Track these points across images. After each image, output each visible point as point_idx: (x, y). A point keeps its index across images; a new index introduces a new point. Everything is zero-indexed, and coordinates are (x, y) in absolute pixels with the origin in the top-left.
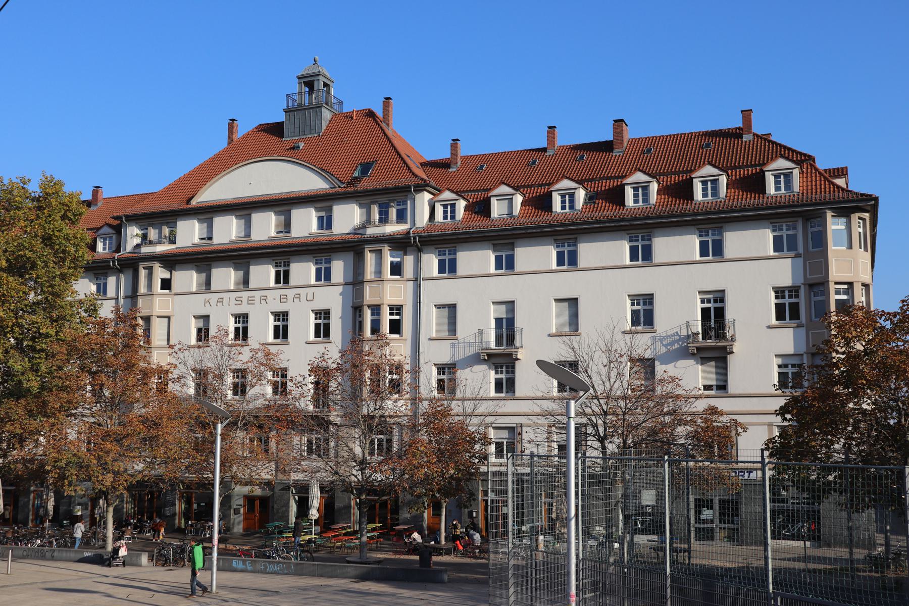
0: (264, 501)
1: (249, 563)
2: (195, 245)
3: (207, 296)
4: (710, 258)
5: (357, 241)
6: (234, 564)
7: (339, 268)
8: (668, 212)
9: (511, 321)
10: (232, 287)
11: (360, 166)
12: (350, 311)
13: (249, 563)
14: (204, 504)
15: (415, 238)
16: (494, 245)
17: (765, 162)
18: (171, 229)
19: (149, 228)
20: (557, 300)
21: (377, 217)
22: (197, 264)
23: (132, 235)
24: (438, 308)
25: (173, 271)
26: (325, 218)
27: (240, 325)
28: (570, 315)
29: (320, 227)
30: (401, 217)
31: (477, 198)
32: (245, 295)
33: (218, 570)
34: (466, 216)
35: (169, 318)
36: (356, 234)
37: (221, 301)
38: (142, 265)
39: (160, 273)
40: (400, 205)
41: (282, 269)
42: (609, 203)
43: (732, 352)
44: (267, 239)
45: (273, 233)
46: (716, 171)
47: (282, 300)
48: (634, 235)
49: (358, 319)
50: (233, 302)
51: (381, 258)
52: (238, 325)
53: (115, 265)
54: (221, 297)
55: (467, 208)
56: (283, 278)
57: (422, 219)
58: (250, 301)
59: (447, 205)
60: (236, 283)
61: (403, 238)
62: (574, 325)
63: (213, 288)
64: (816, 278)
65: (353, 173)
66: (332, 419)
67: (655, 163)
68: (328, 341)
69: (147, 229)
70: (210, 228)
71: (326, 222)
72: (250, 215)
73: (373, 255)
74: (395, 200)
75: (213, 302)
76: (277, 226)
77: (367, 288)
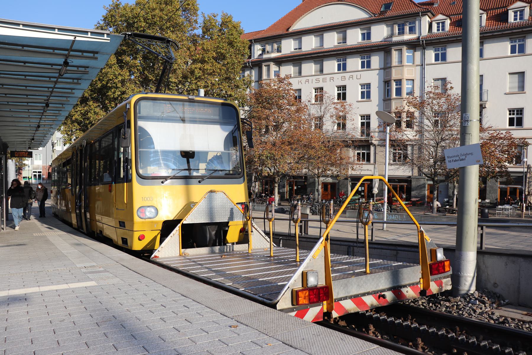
0: (333, 185)
1: (376, 215)
2: (292, 52)
3: (300, 79)
4: (440, 62)
5: (388, 45)
7: (376, 60)
8: (504, 28)
10: (313, 74)
11: (383, 5)
12: (382, 84)
13: (376, 215)
14: (300, 187)
15: (423, 41)
17: (507, 5)
20: (510, 74)
21: (397, 31)
23: (257, 49)
24: (435, 81)
26: (366, 34)
27: (341, 92)
29: (364, 39)
30: (412, 30)
31: (456, 19)
32: (321, 77)
34: (451, 29)
35: (413, 80)
36: (385, 41)
38: (264, 64)
39: (274, 68)
40: (411, 24)
41: (341, 63)
42: (498, 22)
44: (333, 47)
45: (336, 44)
46: (444, 17)
47: (342, 79)
49: (387, 88)
50: (314, 81)
51: (402, 54)
52: (339, 92)
53: (250, 65)
55: (451, 25)
56: (342, 68)
57: (425, 32)
58: (324, 80)
59: (439, 23)
60: (315, 72)
61: (415, 42)
62: (522, 87)
63: (303, 74)
64: (387, 78)
65: (380, 9)
66: (373, 142)
67: (484, 4)
68: (369, 100)
69: (265, 46)
70: (300, 43)
71: (367, 36)
72: (301, 38)
73: (397, 52)
74: (408, 21)
75: (303, 82)
76: (338, 40)
77: (394, 70)
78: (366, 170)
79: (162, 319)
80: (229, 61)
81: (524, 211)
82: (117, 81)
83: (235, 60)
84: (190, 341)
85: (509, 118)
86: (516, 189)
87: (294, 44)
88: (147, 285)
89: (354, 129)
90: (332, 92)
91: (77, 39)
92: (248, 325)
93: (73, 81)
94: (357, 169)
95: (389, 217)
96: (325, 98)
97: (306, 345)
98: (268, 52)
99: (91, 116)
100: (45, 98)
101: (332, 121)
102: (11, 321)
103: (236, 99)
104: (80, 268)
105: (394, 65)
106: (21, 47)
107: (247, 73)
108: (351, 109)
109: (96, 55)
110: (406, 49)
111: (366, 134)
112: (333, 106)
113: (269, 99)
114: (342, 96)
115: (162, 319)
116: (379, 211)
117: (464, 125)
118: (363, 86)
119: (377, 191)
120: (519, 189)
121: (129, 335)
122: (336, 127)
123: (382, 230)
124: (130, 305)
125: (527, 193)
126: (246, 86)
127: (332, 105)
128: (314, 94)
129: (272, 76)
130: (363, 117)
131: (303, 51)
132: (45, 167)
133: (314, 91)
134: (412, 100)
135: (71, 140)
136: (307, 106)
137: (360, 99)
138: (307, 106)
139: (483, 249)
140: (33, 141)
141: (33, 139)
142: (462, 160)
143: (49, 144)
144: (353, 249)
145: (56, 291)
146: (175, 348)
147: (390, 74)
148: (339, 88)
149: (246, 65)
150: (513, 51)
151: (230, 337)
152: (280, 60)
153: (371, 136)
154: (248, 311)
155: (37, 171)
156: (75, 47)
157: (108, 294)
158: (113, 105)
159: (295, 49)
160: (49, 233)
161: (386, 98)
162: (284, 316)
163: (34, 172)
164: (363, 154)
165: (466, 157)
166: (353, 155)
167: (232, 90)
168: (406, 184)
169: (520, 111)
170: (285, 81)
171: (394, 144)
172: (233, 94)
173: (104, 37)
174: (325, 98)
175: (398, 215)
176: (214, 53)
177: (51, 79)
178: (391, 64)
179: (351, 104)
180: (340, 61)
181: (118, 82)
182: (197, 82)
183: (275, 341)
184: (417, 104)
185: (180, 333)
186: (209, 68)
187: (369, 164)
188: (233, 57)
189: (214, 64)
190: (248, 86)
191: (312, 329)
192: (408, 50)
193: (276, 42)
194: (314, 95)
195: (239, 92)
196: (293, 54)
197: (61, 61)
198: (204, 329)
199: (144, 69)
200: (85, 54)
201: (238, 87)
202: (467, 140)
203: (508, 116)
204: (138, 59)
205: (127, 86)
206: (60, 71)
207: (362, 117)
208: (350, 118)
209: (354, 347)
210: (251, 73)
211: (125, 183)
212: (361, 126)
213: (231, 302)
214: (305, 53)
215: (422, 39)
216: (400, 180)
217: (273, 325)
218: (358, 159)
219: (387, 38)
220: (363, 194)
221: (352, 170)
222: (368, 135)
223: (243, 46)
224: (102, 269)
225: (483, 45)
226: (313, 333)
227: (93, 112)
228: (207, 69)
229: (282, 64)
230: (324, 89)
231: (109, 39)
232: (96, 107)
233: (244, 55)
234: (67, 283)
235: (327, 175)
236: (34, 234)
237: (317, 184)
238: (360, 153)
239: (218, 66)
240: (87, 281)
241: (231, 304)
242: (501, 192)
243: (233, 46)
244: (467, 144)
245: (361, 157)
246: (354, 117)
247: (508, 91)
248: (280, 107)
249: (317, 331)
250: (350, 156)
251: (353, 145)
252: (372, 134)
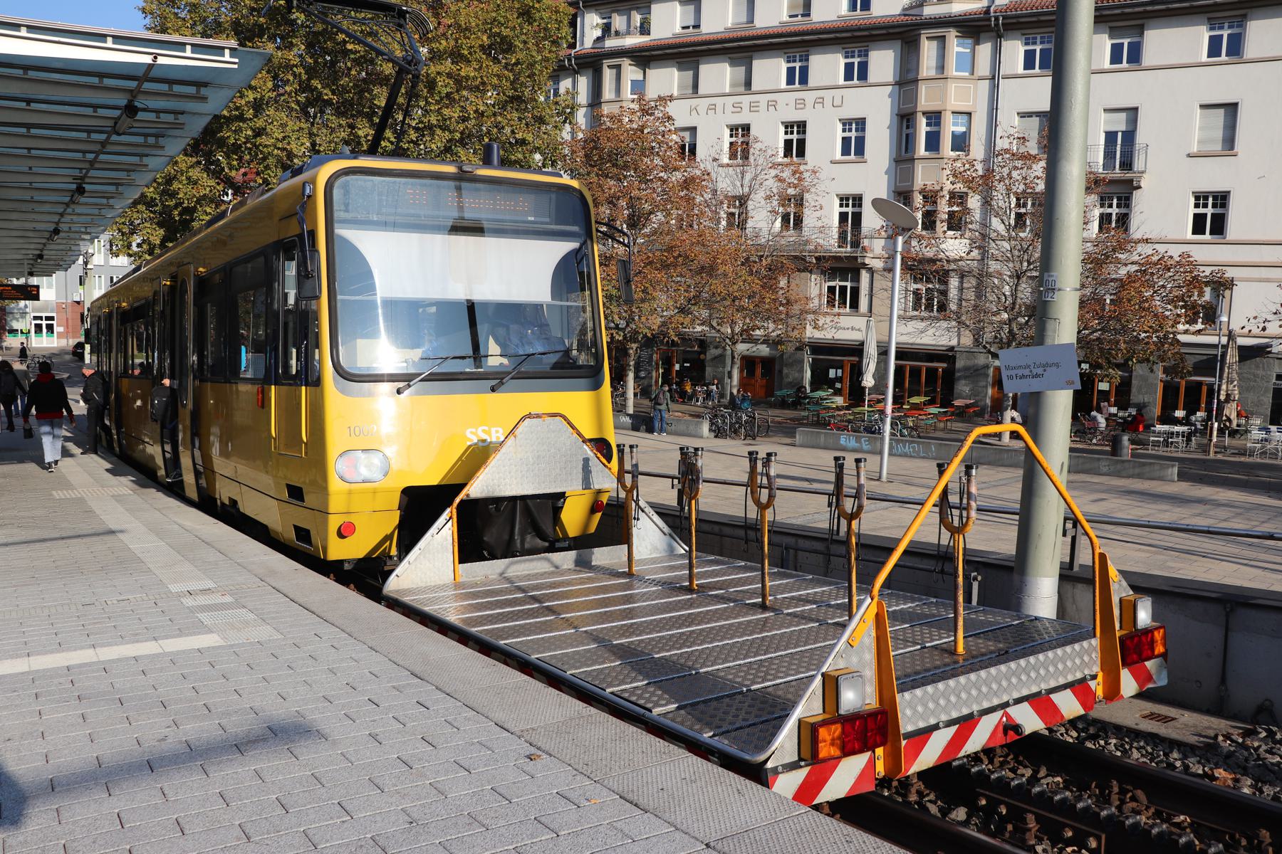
0: (768, 363)
1: (865, 441)
2: (676, 36)
5: (911, 25)
6: (843, 441)
7: (883, 62)
9: (1130, 136)
10: (727, 91)
13: (865, 441)
14: (688, 365)
15: (997, 19)
16: (1111, 28)
18: (645, 16)
19: (613, 15)
20: (1202, 106)
22: (678, 60)
24: (1021, 117)
25: (647, 70)
28: (1225, 127)
32: (746, 100)
33: (890, 454)
35: (969, 114)
37: (713, 107)
38: (606, 63)
39: (631, 73)
43: (1139, 187)
45: (785, 18)
48: (1031, 36)
49: (905, 131)
50: (729, 108)
52: (789, 137)
54: (822, 96)
58: (753, 107)
60: (732, 85)
63: (701, 91)
64: (907, 107)
66: (867, 261)
69: (610, 17)
73: (934, 43)
75: (702, 110)
77: (923, 89)
78: (848, 329)
79: (373, 736)
80: (521, 56)
81: (1215, 439)
82: (243, 102)
83: (534, 54)
84: (435, 792)
85: (1195, 214)
86: (1200, 384)
87: (683, 14)
88: (335, 644)
89: (822, 230)
90: (771, 138)
91: (161, 60)
92: (553, 754)
93: (146, 142)
94: (825, 326)
95: (898, 450)
96: (754, 154)
97: (667, 804)
98: (617, 33)
99: (179, 189)
100: (77, 173)
101: (770, 209)
102: (52, 738)
103: (537, 149)
104: (179, 595)
105: (925, 75)
106: (21, 72)
107: (565, 84)
108: (816, 180)
109: (204, 91)
110: (956, 37)
111: (852, 243)
112: (773, 172)
113: (617, 155)
114: (796, 148)
115: (373, 736)
116: (873, 433)
117: (1044, 299)
118: (846, 123)
119: (873, 382)
120: (1207, 384)
121: (308, 776)
122: (778, 224)
123: (878, 480)
124: (303, 700)
125: (1222, 398)
126: (562, 118)
127: (771, 171)
128: (727, 140)
129: (627, 93)
130: (844, 200)
131: (704, 32)
132: (64, 306)
133: (727, 132)
134: (962, 169)
135: (129, 246)
136: (708, 174)
137: (838, 156)
138: (708, 174)
139: (1076, 568)
140: (39, 261)
141: (41, 256)
142: (1037, 376)
143: (77, 269)
144: (796, 556)
145: (133, 662)
146: (404, 806)
147: (913, 98)
148: (789, 126)
149: (562, 63)
150: (1214, 50)
151: (514, 783)
152: (647, 54)
153: (864, 248)
154: (553, 717)
155: (44, 315)
156: (153, 74)
157: (251, 671)
158: (235, 163)
159: (684, 28)
160: (90, 490)
161: (903, 157)
162: (626, 733)
163: (35, 318)
164: (843, 289)
165: (1045, 371)
166: (818, 292)
167: (528, 127)
168: (945, 365)
169: (1222, 199)
170: (656, 112)
171: (918, 268)
172: (529, 137)
173: (224, 56)
174: (754, 154)
175: (918, 443)
176: (485, 38)
178: (918, 74)
179: (816, 169)
180: (794, 61)
181: (246, 105)
182: (441, 108)
183: (605, 791)
184: (973, 178)
185: (414, 771)
186: (473, 74)
187: (856, 314)
188: (530, 45)
189: (484, 65)
190: (566, 118)
191: (681, 765)
192: (961, 40)
193: (638, 8)
194: (728, 146)
195: (544, 133)
196: (678, 40)
198: (462, 763)
199: (312, 72)
200: (177, 88)
201: (541, 120)
202: (1049, 333)
203: (1192, 210)
204: (295, 50)
205: (268, 115)
206: (116, 123)
207: (841, 199)
208: (813, 204)
209: (761, 810)
210: (574, 84)
211: (273, 387)
212: (840, 223)
213: (518, 693)
214: (707, 37)
215: (995, 12)
216: (931, 355)
217: (604, 755)
218: (831, 303)
219: (911, 7)
220: (838, 385)
221: (814, 328)
222: (856, 244)
223: (556, 20)
224: (228, 599)
225: (1143, 33)
226: (683, 777)
227: (184, 178)
228: (467, 78)
229: (652, 64)
230: (753, 132)
231: (237, 60)
232: (192, 167)
233: (558, 43)
234: (155, 639)
235: (755, 337)
236: (54, 493)
237: (729, 361)
238: (835, 287)
239: (495, 70)
240: (199, 633)
241: (518, 699)
242: (1165, 389)
243: (530, 20)
244: (1049, 341)
245: (837, 298)
246: (821, 201)
247: (1195, 150)
248: (644, 178)
249: (691, 770)
250: (811, 294)
251: (817, 268)
252: (866, 242)
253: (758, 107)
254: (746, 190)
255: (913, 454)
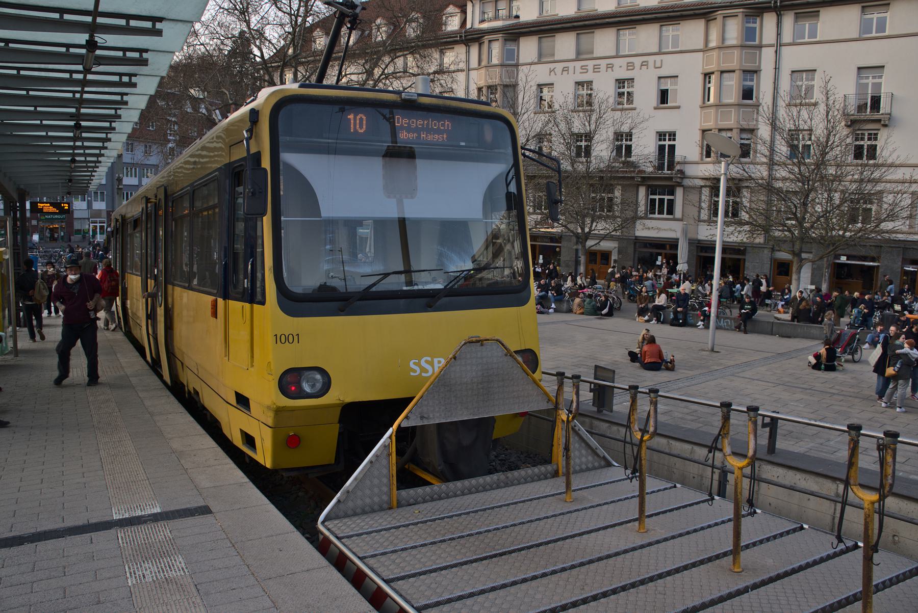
37: (565, 69)
50: (578, 70)
58: (596, 69)
90: (605, 89)
109: (159, 26)
177: (73, 74)
197: (82, 38)
200: (133, 23)
253: (599, 68)
254: (593, 127)
255: (726, 327)
